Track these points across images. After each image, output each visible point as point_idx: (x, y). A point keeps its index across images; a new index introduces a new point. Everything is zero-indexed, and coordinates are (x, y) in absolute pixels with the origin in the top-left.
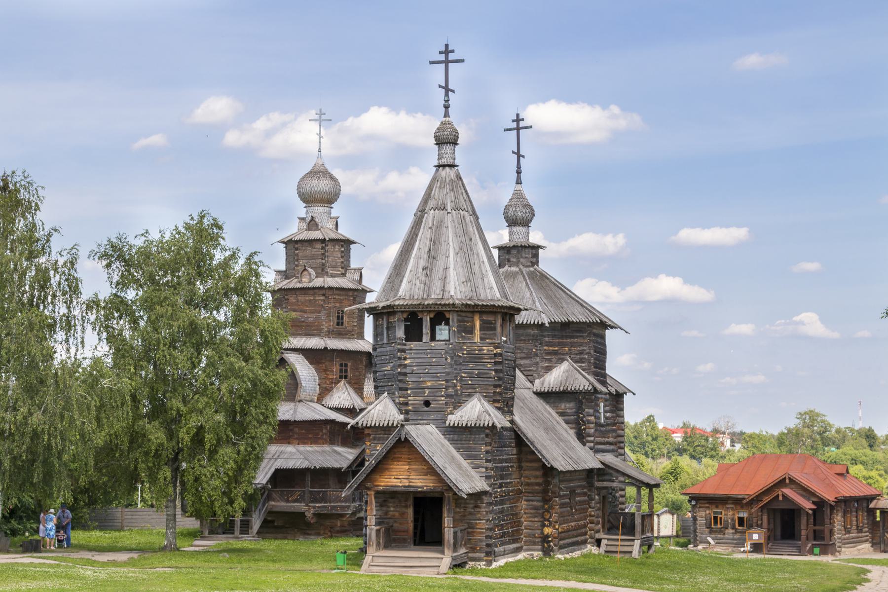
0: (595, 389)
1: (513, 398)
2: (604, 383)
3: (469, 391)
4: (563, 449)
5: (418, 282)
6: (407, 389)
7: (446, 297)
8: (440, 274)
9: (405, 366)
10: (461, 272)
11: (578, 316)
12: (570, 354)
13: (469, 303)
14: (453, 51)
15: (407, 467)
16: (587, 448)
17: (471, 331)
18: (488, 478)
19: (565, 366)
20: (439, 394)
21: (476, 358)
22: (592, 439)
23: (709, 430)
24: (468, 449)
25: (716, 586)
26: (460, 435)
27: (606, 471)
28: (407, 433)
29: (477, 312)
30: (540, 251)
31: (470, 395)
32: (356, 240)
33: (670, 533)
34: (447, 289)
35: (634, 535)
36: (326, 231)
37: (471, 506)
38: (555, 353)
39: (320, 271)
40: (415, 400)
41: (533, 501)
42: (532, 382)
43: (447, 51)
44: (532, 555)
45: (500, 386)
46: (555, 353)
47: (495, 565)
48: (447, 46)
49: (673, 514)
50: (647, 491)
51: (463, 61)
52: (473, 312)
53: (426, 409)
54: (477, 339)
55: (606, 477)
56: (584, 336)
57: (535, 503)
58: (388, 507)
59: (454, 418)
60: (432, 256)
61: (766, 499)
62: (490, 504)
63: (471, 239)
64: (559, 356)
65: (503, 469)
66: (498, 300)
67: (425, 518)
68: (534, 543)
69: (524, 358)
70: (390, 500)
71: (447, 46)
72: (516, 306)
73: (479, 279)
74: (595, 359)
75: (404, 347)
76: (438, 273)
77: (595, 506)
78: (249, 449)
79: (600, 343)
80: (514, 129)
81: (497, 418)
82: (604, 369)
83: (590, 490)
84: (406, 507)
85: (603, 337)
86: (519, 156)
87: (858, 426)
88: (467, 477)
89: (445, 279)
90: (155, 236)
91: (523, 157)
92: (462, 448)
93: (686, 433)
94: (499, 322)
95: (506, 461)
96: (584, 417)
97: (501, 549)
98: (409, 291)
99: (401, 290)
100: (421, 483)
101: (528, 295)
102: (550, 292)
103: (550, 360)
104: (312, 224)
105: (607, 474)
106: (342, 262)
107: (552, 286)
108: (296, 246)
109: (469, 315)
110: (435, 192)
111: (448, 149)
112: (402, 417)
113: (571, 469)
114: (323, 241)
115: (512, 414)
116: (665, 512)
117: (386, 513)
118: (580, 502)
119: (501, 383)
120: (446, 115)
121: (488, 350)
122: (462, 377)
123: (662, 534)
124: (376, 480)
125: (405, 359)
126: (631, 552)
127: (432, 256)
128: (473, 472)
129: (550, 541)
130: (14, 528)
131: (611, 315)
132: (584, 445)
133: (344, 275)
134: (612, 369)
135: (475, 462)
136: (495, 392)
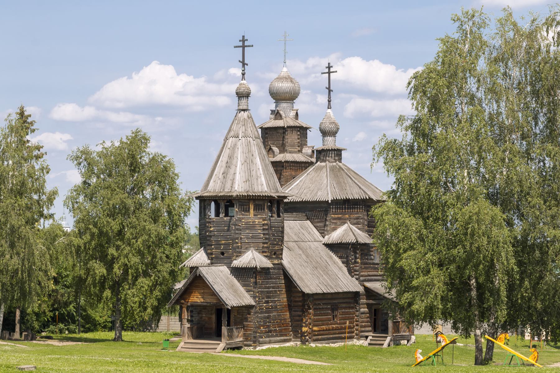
5: (219, 181)
6: (212, 245)
7: (233, 190)
8: (231, 177)
9: (211, 231)
11: (354, 194)
12: (350, 219)
14: (247, 40)
16: (354, 279)
17: (249, 211)
19: (345, 227)
22: (358, 273)
26: (241, 273)
28: (200, 272)
30: (343, 152)
31: (247, 249)
34: (234, 186)
35: (387, 334)
36: (287, 121)
38: (339, 219)
39: (282, 149)
41: (297, 311)
42: (324, 237)
43: (243, 40)
45: (267, 243)
46: (339, 219)
47: (258, 348)
48: (243, 37)
51: (336, 72)
58: (202, 314)
59: (238, 262)
60: (228, 166)
62: (256, 313)
64: (342, 221)
65: (268, 292)
66: (266, 192)
67: (213, 322)
69: (320, 222)
70: (203, 310)
71: (243, 37)
72: (283, 195)
76: (230, 177)
78: (157, 278)
80: (327, 73)
84: (211, 314)
88: (233, 294)
89: (233, 181)
90: (108, 144)
95: (273, 287)
98: (215, 188)
100: (210, 300)
101: (325, 182)
102: (341, 180)
103: (336, 223)
104: (277, 115)
106: (299, 142)
107: (344, 175)
108: (266, 131)
110: (234, 127)
111: (244, 101)
112: (209, 261)
113: (320, 292)
114: (283, 128)
115: (282, 259)
117: (201, 318)
119: (267, 241)
121: (259, 222)
122: (241, 238)
125: (211, 227)
127: (228, 166)
128: (246, 294)
129: (305, 336)
130: (16, 325)
132: (353, 277)
133: (300, 151)
135: (248, 288)
136: (263, 247)
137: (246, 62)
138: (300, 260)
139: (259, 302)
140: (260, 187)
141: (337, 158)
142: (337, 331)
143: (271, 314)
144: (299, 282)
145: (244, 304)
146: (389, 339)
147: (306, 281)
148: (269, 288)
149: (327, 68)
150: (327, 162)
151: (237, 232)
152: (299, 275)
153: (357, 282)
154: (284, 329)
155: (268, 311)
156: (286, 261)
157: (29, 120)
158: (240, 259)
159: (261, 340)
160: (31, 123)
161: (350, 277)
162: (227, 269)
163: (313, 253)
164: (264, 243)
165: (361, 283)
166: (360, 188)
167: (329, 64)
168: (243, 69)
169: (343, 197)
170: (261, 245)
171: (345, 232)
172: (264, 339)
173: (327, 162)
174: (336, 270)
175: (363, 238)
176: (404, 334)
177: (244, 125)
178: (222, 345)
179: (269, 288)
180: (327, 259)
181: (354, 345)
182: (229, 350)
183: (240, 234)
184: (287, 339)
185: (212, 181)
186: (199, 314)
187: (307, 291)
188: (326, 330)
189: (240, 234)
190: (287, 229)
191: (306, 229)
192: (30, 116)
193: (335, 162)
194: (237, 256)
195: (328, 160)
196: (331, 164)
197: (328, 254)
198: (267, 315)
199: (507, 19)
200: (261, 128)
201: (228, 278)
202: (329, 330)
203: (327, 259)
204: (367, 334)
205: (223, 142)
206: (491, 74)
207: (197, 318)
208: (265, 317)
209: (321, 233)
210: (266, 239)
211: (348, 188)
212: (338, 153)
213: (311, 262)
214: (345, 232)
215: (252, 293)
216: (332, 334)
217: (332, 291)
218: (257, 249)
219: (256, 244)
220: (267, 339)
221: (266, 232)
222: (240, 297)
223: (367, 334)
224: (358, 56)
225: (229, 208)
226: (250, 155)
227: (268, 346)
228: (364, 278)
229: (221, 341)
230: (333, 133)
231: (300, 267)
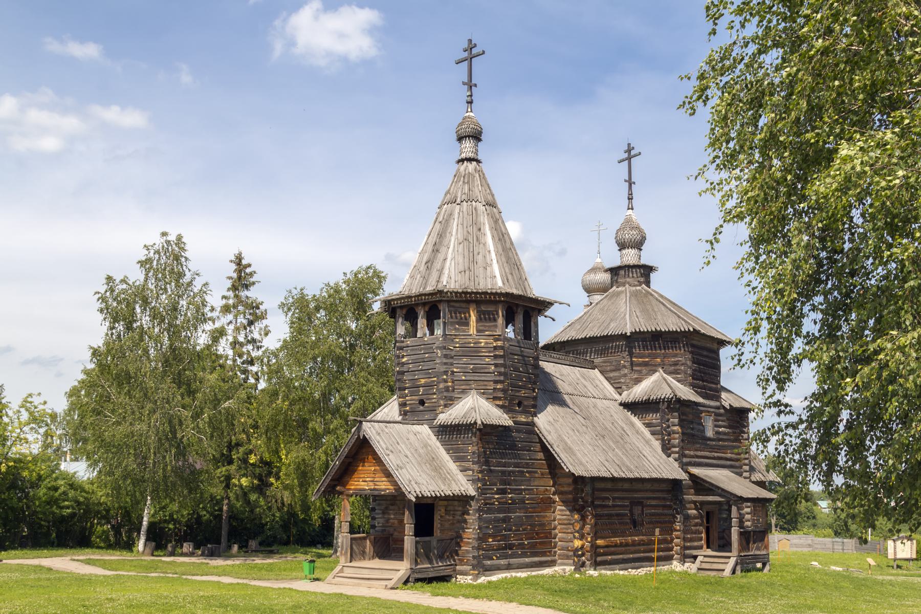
3: (463, 387)
9: (403, 364)
10: (461, 261)
11: (670, 324)
17: (467, 324)
18: (474, 481)
20: (431, 392)
21: (473, 352)
24: (456, 451)
31: (464, 392)
33: (909, 556)
34: (441, 280)
37: (459, 513)
38: (646, 364)
40: (412, 400)
42: (621, 395)
44: (564, 570)
46: (646, 364)
51: (640, 154)
52: (469, 302)
53: (421, 408)
54: (472, 330)
58: (389, 514)
59: (447, 416)
63: (480, 230)
65: (503, 472)
68: (568, 557)
70: (391, 507)
73: (481, 269)
76: (437, 265)
83: (675, 504)
92: (452, 449)
96: (668, 427)
100: (384, 486)
103: (640, 372)
107: (654, 302)
109: (464, 305)
117: (388, 520)
119: (502, 378)
121: (486, 343)
122: (453, 372)
123: (898, 556)
124: (347, 483)
132: (669, 456)
135: (463, 464)
136: (495, 389)
138: (573, 422)
139: (482, 491)
141: (642, 280)
142: (642, 548)
143: (513, 515)
145: (448, 493)
146: (732, 561)
147: (579, 455)
150: (627, 286)
152: (566, 443)
153: (676, 464)
154: (540, 543)
155: (505, 507)
157: (248, 270)
160: (251, 275)
161: (664, 456)
162: (429, 430)
163: (599, 416)
164: (496, 382)
165: (683, 466)
166: (679, 317)
167: (629, 145)
168: (469, 93)
169: (651, 327)
170: (491, 386)
171: (655, 384)
172: (496, 562)
173: (627, 286)
174: (640, 445)
175: (686, 393)
176: (758, 553)
177: (468, 182)
180: (624, 426)
181: (673, 572)
182: (420, 584)
184: (546, 562)
186: (383, 513)
187: (579, 471)
188: (621, 545)
191: (591, 380)
192: (249, 265)
193: (640, 285)
194: (446, 406)
196: (634, 288)
197: (628, 419)
201: (426, 445)
202: (627, 545)
203: (624, 426)
204: (695, 552)
207: (381, 521)
208: (497, 520)
209: (616, 388)
210: (500, 374)
211: (659, 318)
212: (646, 271)
213: (594, 426)
214: (655, 384)
215: (470, 473)
216: (632, 553)
217: (631, 476)
218: (483, 393)
219: (482, 383)
220: (503, 562)
221: (501, 361)
222: (444, 480)
223: (695, 552)
227: (504, 575)
228: (688, 460)
230: (638, 245)
231: (570, 432)
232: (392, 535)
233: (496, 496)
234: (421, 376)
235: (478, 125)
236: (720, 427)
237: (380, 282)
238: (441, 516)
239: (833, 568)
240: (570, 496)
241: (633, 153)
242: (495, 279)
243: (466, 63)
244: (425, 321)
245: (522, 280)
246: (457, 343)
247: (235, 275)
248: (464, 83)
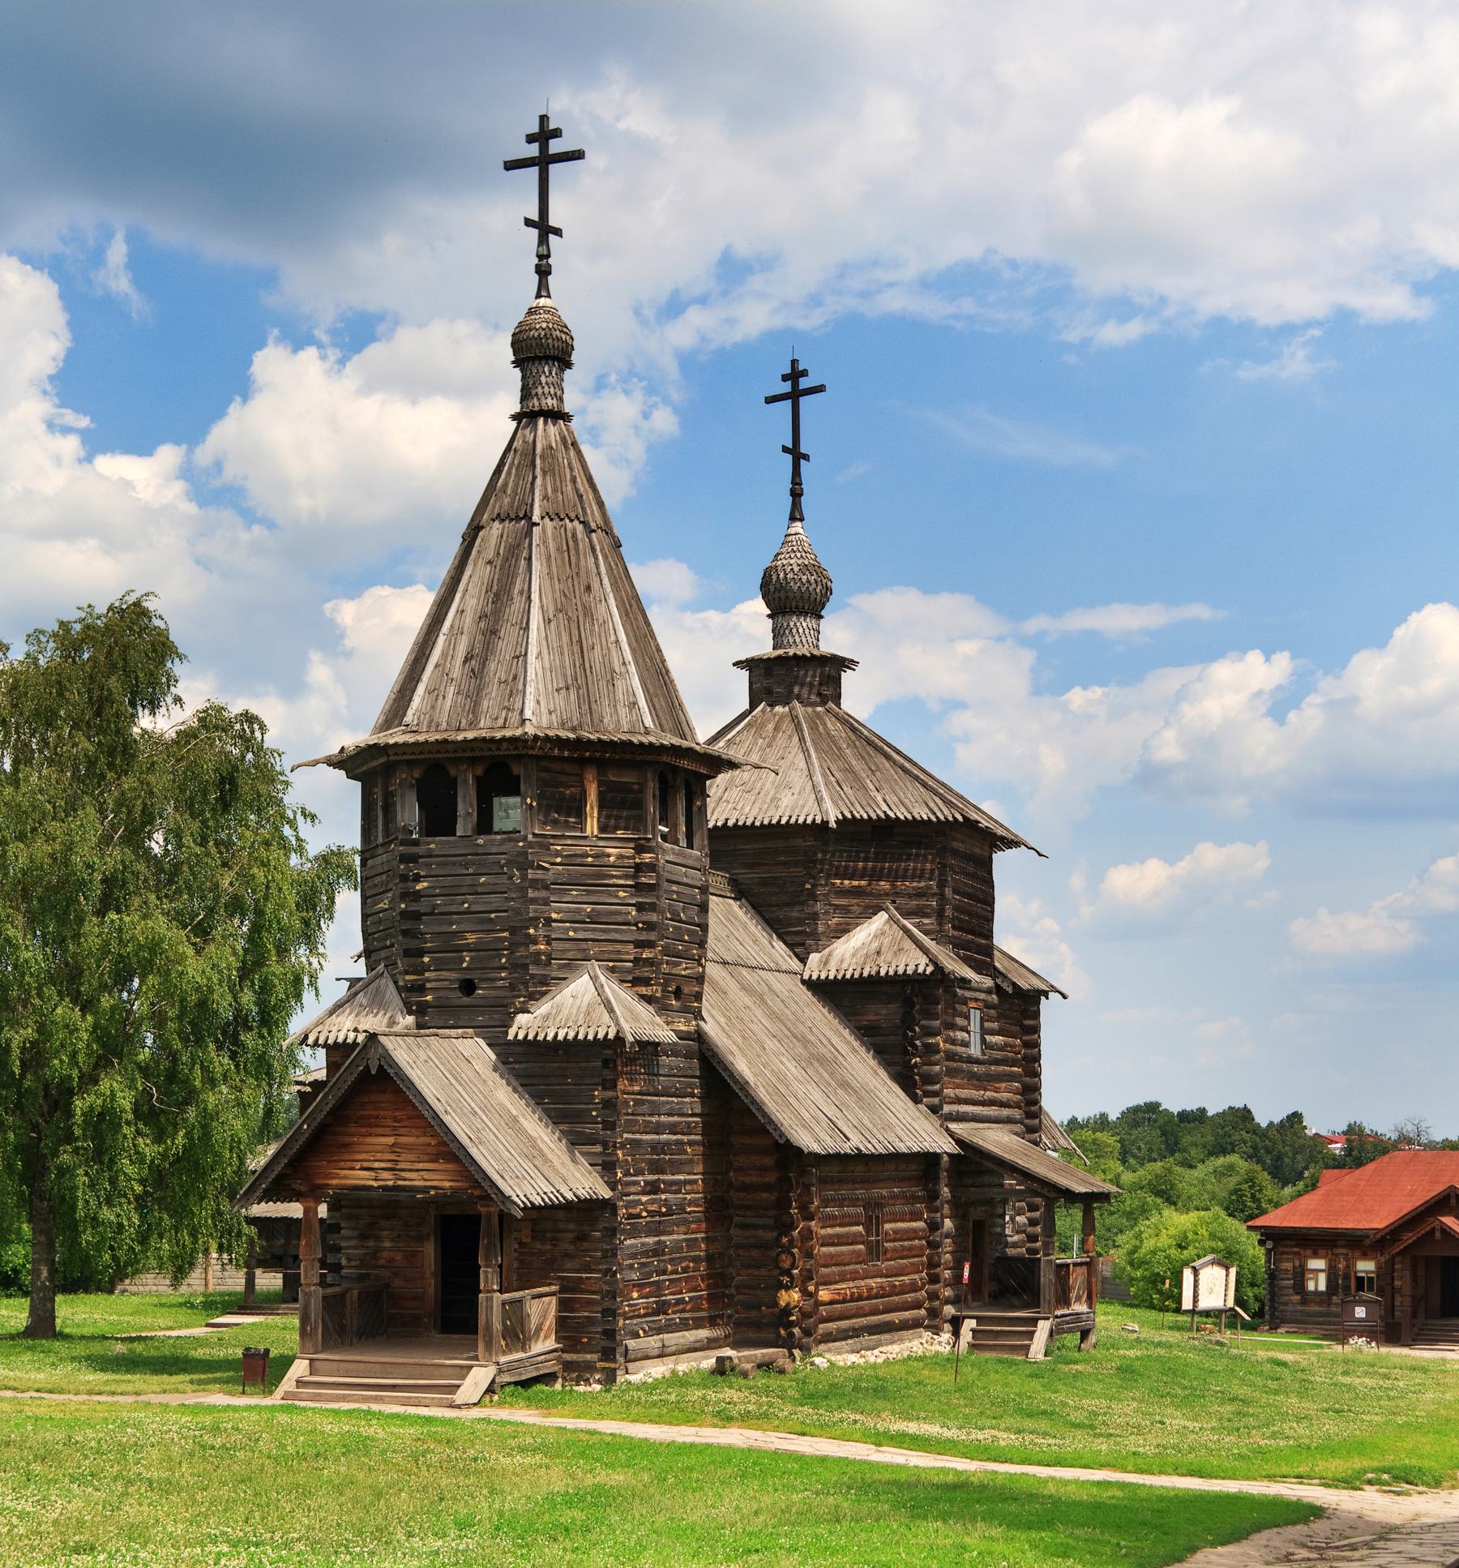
0: (939, 968)
1: (700, 979)
2: (984, 965)
4: (832, 1098)
9: (418, 896)
11: (916, 807)
12: (894, 895)
13: (564, 734)
15: (391, 1140)
16: (922, 1107)
17: (577, 810)
23: (311, 353)
25: (6, 875)
27: (972, 1163)
29: (591, 761)
31: (571, 967)
32: (1023, 835)
37: (570, 1235)
41: (755, 1227)
42: (803, 960)
43: (795, 374)
45: (651, 944)
48: (543, 119)
49: (1227, 1269)
50: (1077, 1213)
52: (582, 762)
53: (466, 1000)
54: (592, 826)
55: (986, 1179)
56: (945, 858)
57: (760, 1233)
58: (379, 1239)
59: (524, 1025)
60: (490, 625)
61: (1409, 1238)
65: (657, 1148)
67: (411, 1270)
71: (543, 119)
73: (603, 683)
74: (956, 908)
75: (414, 850)
76: (497, 669)
77: (995, 1245)
79: (979, 907)
81: (613, 992)
82: (989, 935)
84: (420, 1239)
85: (987, 866)
86: (796, 453)
87: (1371, 1167)
88: (530, 1161)
91: (529, 223)
93: (1349, 1141)
94: (652, 787)
95: (673, 1129)
97: (652, 1342)
99: (410, 712)
100: (428, 1178)
103: (845, 910)
105: (981, 1173)
111: (546, 374)
115: (698, 1015)
116: (1213, 1263)
117: (375, 1254)
118: (899, 1235)
119: (652, 936)
120: (543, 290)
121: (620, 857)
122: (549, 921)
123: (1204, 1304)
125: (417, 878)
126: (1028, 1347)
129: (792, 1324)
131: (994, 810)
132: (916, 1100)
134: (1007, 938)
136: (636, 961)
137: (553, 222)
140: (623, 711)
144: (772, 1107)
148: (658, 1129)
149: (785, 378)
150: (796, 703)
151: (531, 894)
156: (710, 1028)
158: (543, 1008)
159: (632, 1344)
164: (640, 944)
167: (794, 362)
178: (480, 1376)
179: (658, 1129)
180: (829, 1034)
183: (546, 902)
185: (421, 689)
186: (363, 1237)
189: (546, 902)
190: (711, 905)
195: (798, 697)
198: (651, 1240)
199: (534, 1112)
200: (351, 763)
205: (454, 546)
206: (1272, 1276)
212: (830, 670)
215: (598, 1149)
219: (610, 947)
224: (1436, 600)
225: (496, 800)
226: (580, 589)
229: (476, 1358)
232: (387, 1286)
233: (644, 1199)
234: (463, 927)
235: (817, 569)
236: (993, 1033)
237: (247, 742)
238: (521, 1244)
239: (966, 1274)
240: (955, 845)
241: (804, 383)
242: (629, 717)
243: (787, 405)
244: (473, 793)
245: (680, 725)
246: (558, 854)
247: (1424, 1140)
248: (785, 449)
